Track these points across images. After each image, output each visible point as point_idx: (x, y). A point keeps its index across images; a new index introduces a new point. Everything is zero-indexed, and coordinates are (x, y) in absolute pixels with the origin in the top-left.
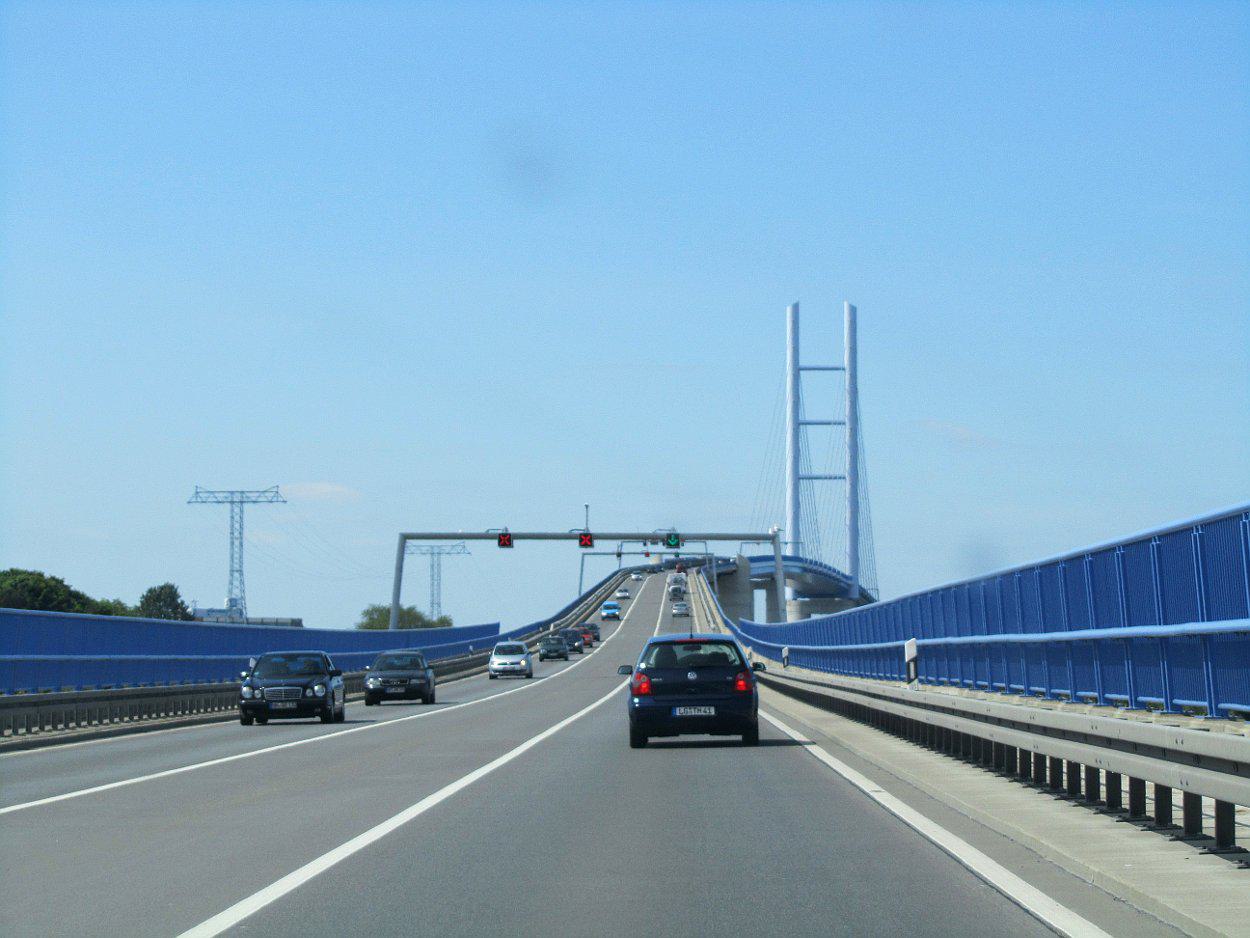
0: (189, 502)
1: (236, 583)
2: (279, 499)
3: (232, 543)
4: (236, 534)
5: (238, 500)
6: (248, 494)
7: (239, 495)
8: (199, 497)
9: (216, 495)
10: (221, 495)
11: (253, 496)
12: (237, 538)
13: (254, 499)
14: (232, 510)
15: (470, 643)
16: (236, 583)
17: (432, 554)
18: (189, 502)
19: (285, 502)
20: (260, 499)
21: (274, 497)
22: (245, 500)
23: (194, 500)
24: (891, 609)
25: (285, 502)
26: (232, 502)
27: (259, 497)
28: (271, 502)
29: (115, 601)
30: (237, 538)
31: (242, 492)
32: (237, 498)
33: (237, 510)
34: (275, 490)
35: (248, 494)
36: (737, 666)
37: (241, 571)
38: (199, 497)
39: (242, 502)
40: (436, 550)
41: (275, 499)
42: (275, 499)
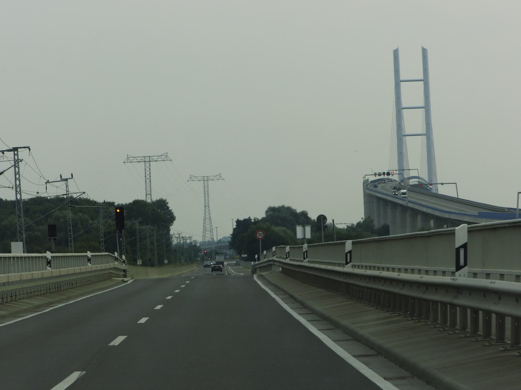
0: (124, 163)
1: (207, 210)
2: (168, 159)
3: (205, 196)
4: (206, 192)
5: (147, 160)
6: (153, 158)
7: (148, 158)
8: (129, 160)
9: (198, 178)
10: (199, 178)
11: (155, 158)
12: (206, 193)
13: (156, 160)
14: (204, 184)
15: (119, 239)
16: (207, 210)
17: (204, 180)
18: (124, 163)
19: (171, 160)
20: (158, 160)
21: (165, 157)
22: (209, 179)
23: (126, 161)
24: (368, 191)
25: (171, 160)
26: (145, 162)
27: (214, 178)
28: (218, 180)
29: (313, 220)
30: (206, 193)
31: (150, 157)
32: (206, 178)
33: (147, 165)
34: (220, 175)
35: (153, 158)
36: (252, 222)
37: (151, 194)
38: (129, 160)
39: (149, 161)
40: (206, 178)
41: (166, 159)
42: (166, 159)
